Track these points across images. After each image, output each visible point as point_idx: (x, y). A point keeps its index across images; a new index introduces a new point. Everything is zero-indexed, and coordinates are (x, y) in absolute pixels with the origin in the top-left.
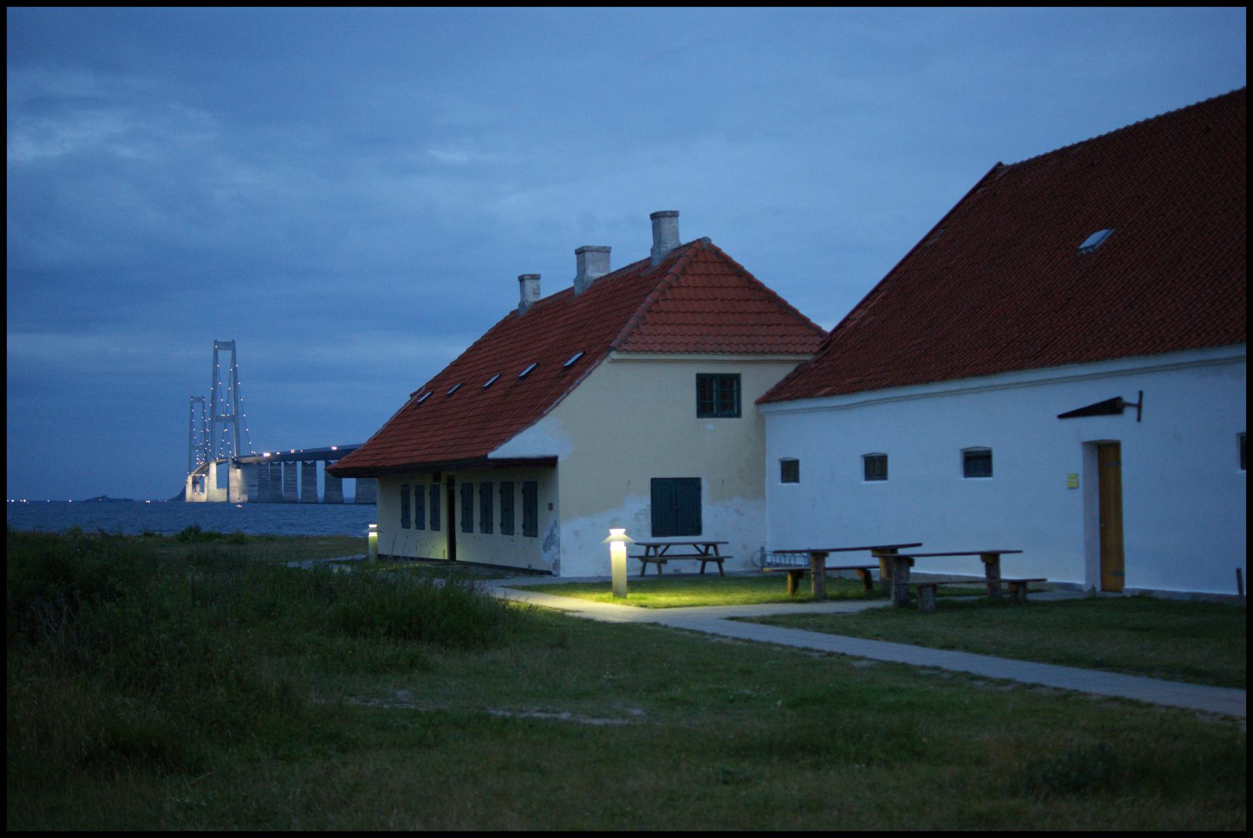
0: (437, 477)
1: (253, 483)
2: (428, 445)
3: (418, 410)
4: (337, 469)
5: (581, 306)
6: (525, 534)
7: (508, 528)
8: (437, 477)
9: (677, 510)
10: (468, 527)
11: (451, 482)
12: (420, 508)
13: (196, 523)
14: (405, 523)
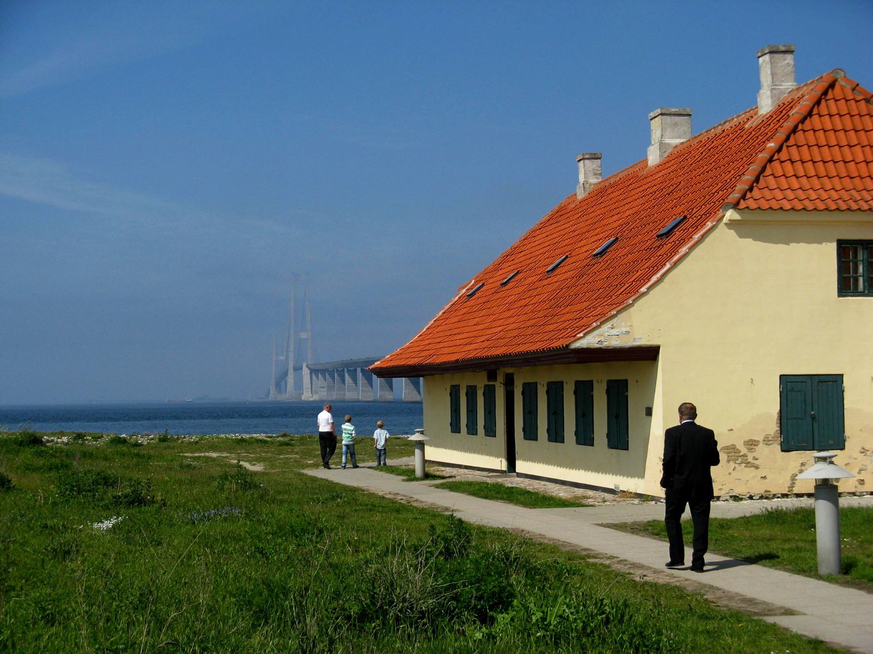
0: (492, 376)
1: (579, 159)
2: (482, 339)
3: (468, 302)
4: (381, 368)
5: (660, 174)
6: (611, 446)
7: (585, 437)
8: (492, 376)
9: (813, 418)
10: (531, 434)
11: (509, 382)
12: (530, 412)
13: (792, 73)
14: (455, 428)
